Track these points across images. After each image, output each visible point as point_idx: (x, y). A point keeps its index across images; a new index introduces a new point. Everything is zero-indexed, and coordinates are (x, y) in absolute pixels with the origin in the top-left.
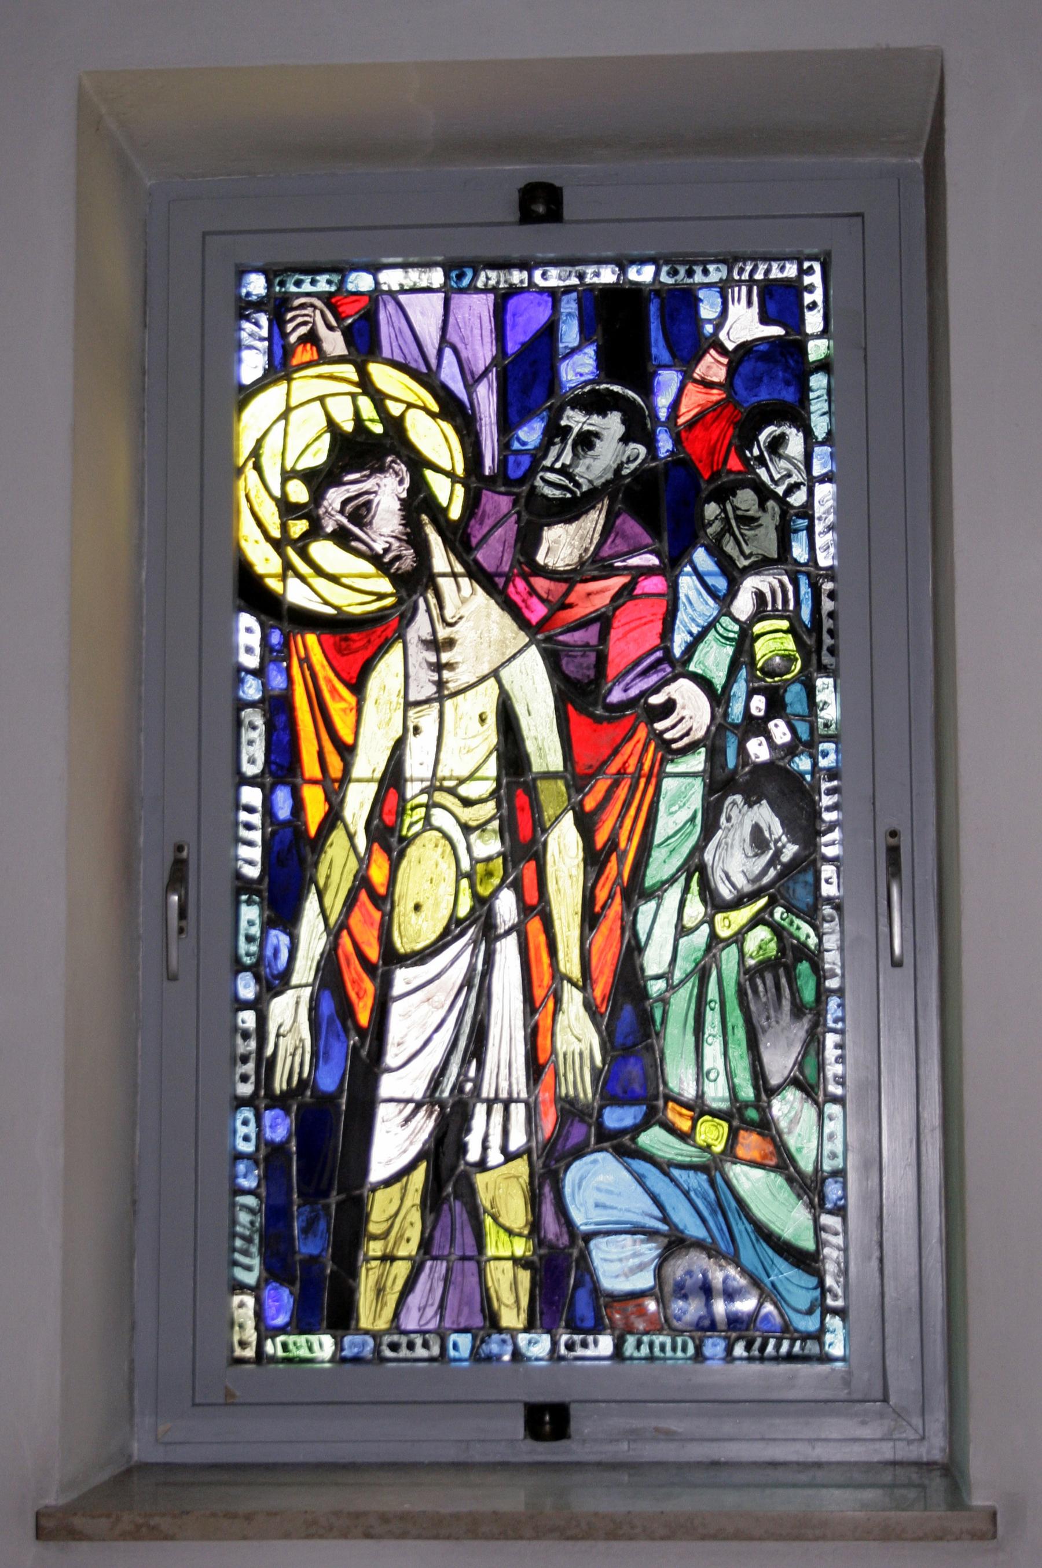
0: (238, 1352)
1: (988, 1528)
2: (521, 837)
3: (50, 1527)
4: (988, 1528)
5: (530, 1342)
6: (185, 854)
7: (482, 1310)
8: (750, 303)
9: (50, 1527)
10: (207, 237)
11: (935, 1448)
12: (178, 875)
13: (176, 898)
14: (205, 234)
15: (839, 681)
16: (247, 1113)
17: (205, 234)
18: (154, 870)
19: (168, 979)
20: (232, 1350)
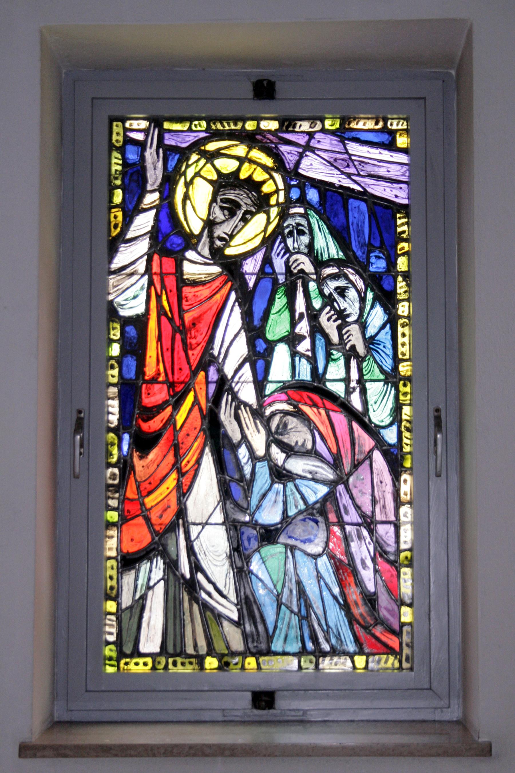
0: (111, 482)
1: (486, 751)
2: (234, 441)
3: (26, 750)
4: (486, 751)
5: (355, 487)
6: (82, 415)
7: (326, 441)
8: (259, 431)
9: (26, 750)
10: (94, 100)
11: (454, 713)
12: (79, 426)
13: (79, 437)
14: (93, 99)
15: (215, 671)
16: (113, 532)
17: (93, 99)
18: (67, 425)
19: (74, 477)
20: (106, 481)
